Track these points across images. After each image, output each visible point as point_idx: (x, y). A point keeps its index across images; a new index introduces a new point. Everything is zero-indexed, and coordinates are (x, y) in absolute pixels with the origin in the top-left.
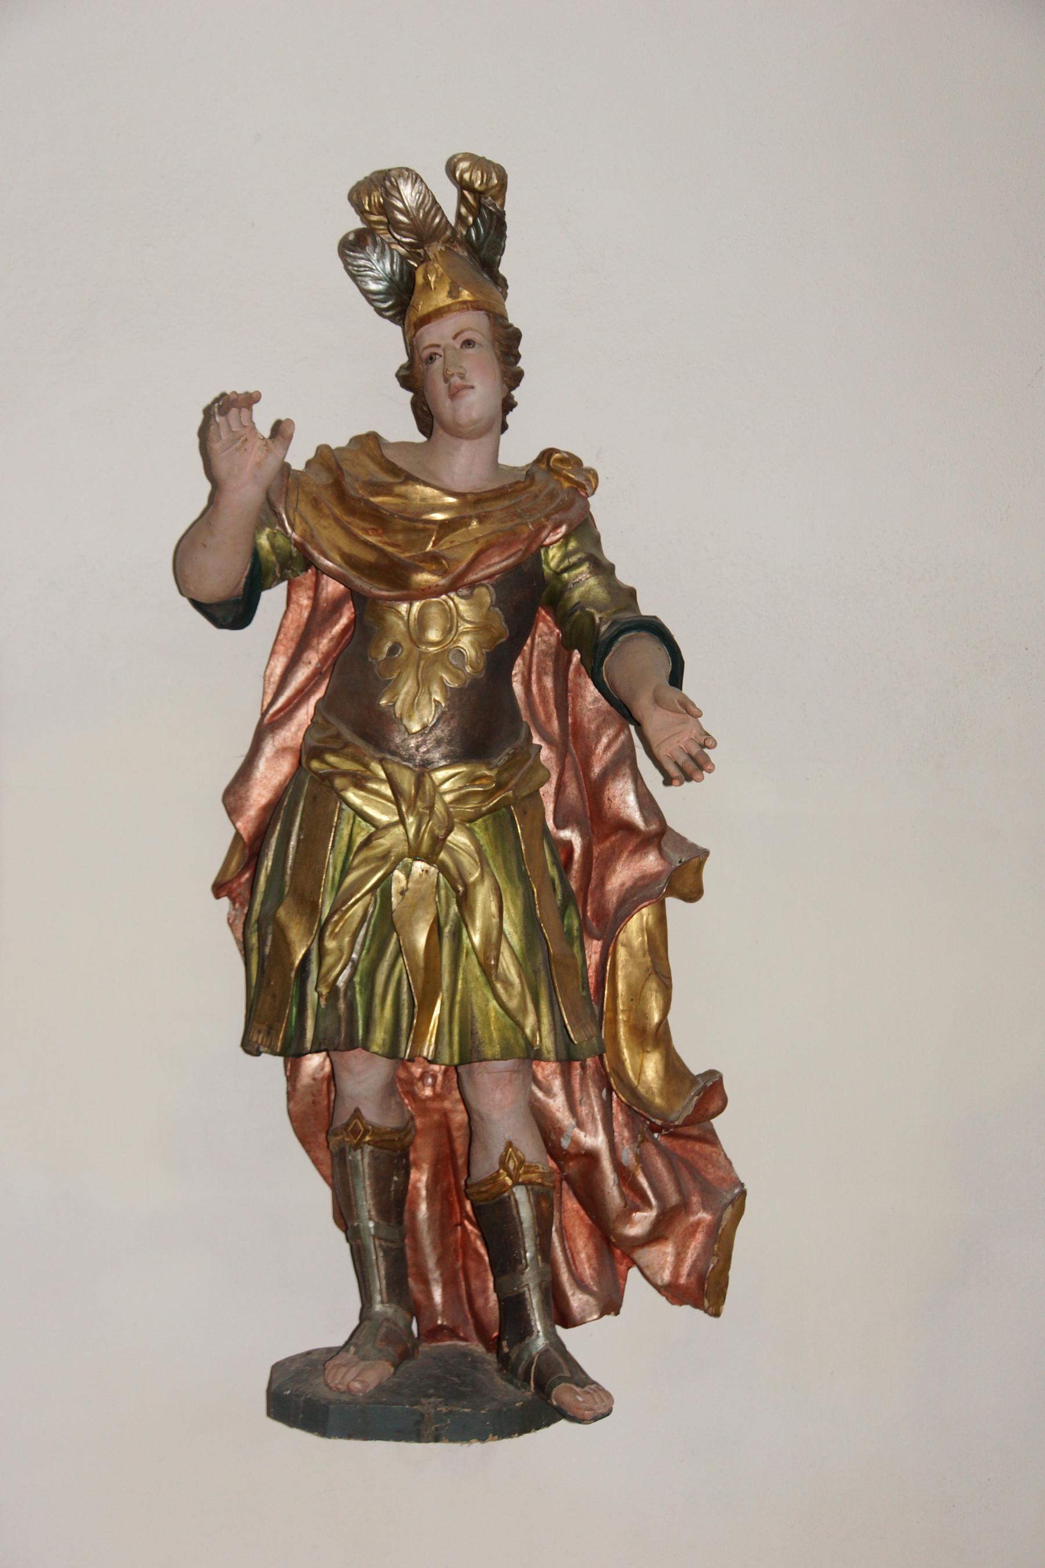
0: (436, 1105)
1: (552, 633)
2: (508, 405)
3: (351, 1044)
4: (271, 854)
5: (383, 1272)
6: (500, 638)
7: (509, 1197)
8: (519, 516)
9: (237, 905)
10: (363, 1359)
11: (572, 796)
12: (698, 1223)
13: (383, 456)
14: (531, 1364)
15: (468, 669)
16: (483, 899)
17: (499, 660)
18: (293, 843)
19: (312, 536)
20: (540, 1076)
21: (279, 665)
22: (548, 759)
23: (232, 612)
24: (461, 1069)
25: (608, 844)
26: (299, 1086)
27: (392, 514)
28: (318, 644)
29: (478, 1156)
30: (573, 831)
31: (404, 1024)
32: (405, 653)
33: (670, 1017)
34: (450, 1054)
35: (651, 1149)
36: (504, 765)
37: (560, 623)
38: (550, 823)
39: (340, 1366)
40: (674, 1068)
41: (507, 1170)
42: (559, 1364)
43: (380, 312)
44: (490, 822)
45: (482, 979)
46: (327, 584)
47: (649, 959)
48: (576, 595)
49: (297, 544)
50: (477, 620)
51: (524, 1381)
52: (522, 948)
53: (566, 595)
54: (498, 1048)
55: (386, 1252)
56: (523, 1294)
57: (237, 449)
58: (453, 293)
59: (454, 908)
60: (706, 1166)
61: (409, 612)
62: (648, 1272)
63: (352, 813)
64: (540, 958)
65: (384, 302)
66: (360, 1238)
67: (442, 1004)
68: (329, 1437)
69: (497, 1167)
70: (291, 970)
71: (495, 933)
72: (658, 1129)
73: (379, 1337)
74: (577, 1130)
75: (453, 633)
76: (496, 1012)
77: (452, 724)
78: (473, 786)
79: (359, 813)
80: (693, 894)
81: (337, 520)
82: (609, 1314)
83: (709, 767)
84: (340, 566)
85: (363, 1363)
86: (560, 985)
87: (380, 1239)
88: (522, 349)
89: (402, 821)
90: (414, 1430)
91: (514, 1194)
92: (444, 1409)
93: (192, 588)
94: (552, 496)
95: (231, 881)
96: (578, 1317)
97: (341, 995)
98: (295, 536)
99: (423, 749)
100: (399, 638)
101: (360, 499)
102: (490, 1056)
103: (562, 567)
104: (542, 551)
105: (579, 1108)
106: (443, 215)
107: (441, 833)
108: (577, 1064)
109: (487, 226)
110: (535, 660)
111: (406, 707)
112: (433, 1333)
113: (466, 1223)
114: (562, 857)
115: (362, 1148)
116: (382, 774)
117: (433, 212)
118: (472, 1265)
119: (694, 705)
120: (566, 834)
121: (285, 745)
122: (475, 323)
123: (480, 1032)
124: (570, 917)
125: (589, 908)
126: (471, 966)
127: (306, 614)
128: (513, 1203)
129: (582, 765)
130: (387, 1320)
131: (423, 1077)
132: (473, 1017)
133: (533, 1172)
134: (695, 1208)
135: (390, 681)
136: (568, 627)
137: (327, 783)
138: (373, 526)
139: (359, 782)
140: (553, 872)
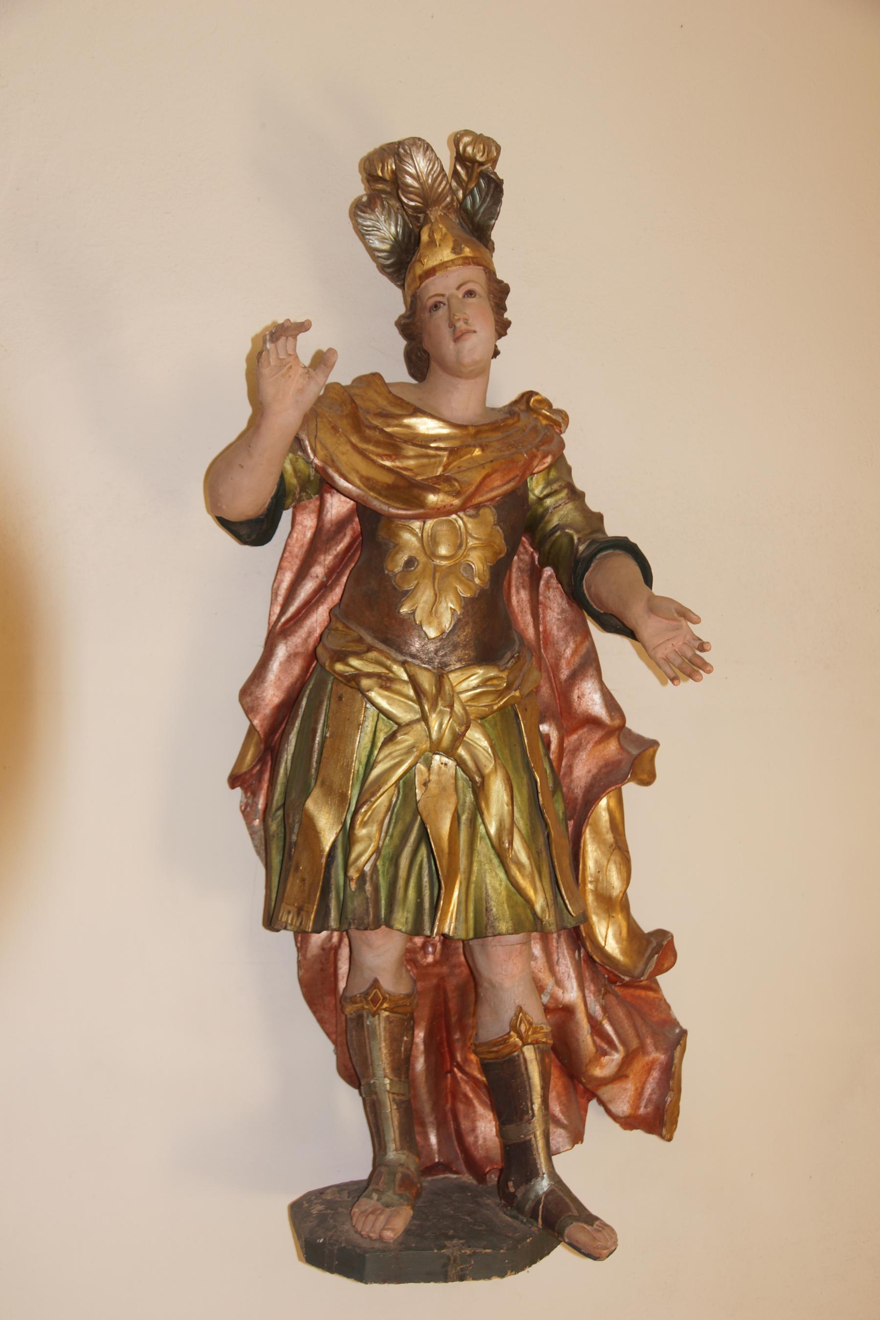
5: (396, 1123)
6: (500, 553)
7: (518, 1056)
9: (249, 794)
10: (387, 1206)
12: (653, 1062)
13: (390, 392)
14: (539, 1202)
15: (477, 581)
16: (497, 790)
19: (333, 461)
21: (288, 578)
30: (550, 726)
32: (420, 567)
42: (566, 1203)
43: (382, 268)
49: (317, 469)
50: (484, 537)
51: (531, 1217)
55: (399, 1104)
57: (283, 376)
58: (456, 250)
61: (422, 529)
64: (541, 840)
66: (376, 1093)
68: (366, 1283)
73: (397, 1183)
74: (556, 988)
75: (463, 548)
80: (647, 778)
83: (708, 669)
84: (358, 487)
85: (388, 1211)
86: (559, 863)
87: (393, 1093)
89: (424, 718)
90: (441, 1274)
91: (523, 1053)
93: (224, 507)
94: (535, 429)
95: (245, 773)
97: (368, 879)
98: (316, 461)
99: (441, 653)
102: (504, 931)
109: (484, 194)
112: (430, 1169)
113: (455, 1069)
116: (405, 677)
117: (440, 178)
118: (461, 1107)
120: (544, 728)
123: (494, 910)
126: (483, 848)
128: (522, 1060)
130: (402, 1165)
131: (424, 946)
133: (539, 1032)
135: (408, 591)
137: (353, 684)
139: (386, 682)
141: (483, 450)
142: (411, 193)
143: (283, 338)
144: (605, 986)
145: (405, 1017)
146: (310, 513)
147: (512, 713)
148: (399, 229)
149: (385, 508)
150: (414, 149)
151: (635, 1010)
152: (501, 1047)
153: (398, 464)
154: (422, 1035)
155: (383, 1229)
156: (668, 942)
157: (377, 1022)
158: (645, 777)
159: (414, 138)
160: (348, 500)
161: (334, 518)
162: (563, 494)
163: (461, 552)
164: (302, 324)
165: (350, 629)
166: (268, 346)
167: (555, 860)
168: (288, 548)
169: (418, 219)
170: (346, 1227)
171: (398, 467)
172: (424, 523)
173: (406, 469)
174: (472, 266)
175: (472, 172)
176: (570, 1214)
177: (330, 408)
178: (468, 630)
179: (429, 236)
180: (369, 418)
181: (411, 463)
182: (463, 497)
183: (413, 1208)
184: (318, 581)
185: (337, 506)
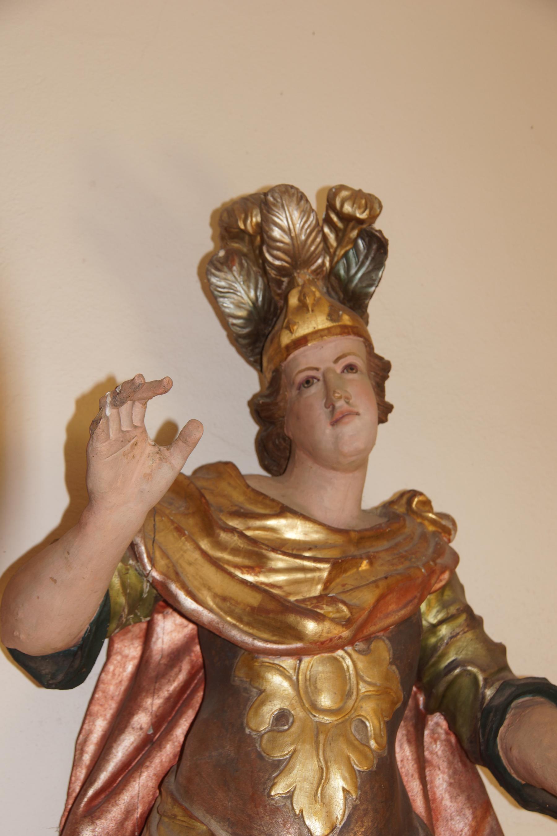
13: (248, 486)
19: (177, 574)
21: (100, 726)
43: (235, 339)
49: (154, 584)
57: (125, 455)
58: (331, 316)
61: (297, 670)
75: (354, 697)
84: (211, 610)
93: (22, 636)
98: (155, 574)
109: (361, 258)
141: (371, 563)
142: (279, 249)
143: (129, 403)
146: (132, 639)
148: (260, 294)
149: (248, 640)
150: (286, 197)
153: (262, 579)
159: (286, 186)
160: (185, 622)
161: (166, 646)
162: (462, 619)
163: (351, 703)
164: (159, 383)
165: (197, 819)
166: (108, 411)
168: (101, 686)
169: (279, 283)
171: (262, 583)
172: (300, 661)
173: (273, 586)
174: (352, 337)
175: (344, 236)
177: (171, 504)
178: (367, 822)
179: (299, 300)
180: (223, 518)
181: (280, 578)
182: (355, 626)
184: (142, 734)
185: (170, 631)
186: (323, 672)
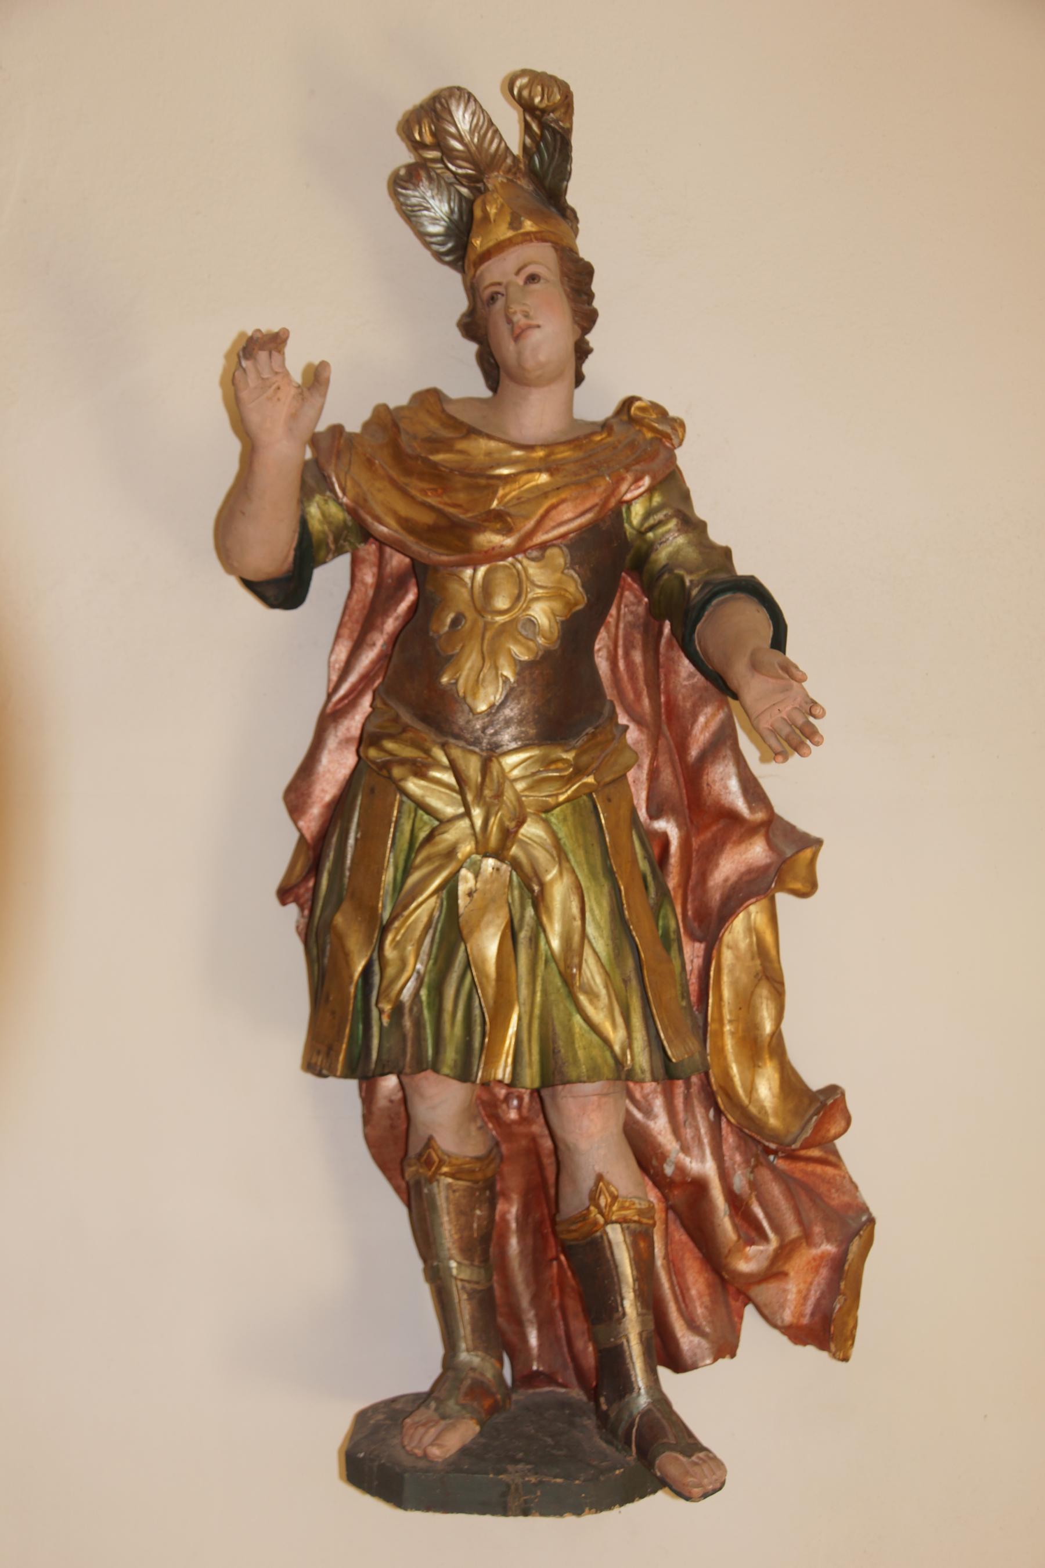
0: (522, 1129)
1: (640, 602)
2: (582, 351)
3: (420, 1065)
4: (332, 855)
6: (576, 604)
8: (592, 467)
10: (443, 1417)
11: (666, 783)
13: (443, 411)
14: (632, 1425)
15: (541, 640)
17: (578, 629)
18: (351, 841)
19: (365, 500)
20: (638, 1095)
21: (342, 653)
22: (637, 742)
23: (284, 590)
24: (546, 1093)
25: (708, 835)
26: (375, 1109)
27: (452, 470)
28: (383, 623)
29: (566, 1190)
30: (668, 821)
31: (477, 1044)
33: (784, 1027)
34: (531, 1077)
35: (765, 1174)
36: (582, 746)
37: (647, 590)
38: (643, 814)
39: (416, 1425)
40: (791, 1083)
41: (598, 1206)
43: (439, 256)
44: (569, 811)
45: (563, 991)
46: (391, 556)
47: (758, 962)
48: (662, 555)
52: (608, 954)
53: (653, 556)
54: (584, 1069)
56: (622, 1344)
57: (269, 399)
58: (515, 223)
59: (530, 911)
60: (829, 1191)
61: (473, 578)
62: (766, 1312)
63: (413, 805)
64: (630, 963)
65: (442, 244)
67: (520, 1019)
68: (405, 1509)
69: (587, 1203)
70: (351, 983)
71: (576, 938)
72: (775, 1152)
74: (682, 1156)
75: (523, 599)
76: (581, 1028)
77: (522, 702)
78: (547, 771)
79: (421, 806)
81: (393, 482)
82: (723, 1357)
83: (816, 739)
84: (396, 531)
85: (443, 1423)
86: (654, 996)
88: (595, 287)
89: (468, 814)
90: (500, 1505)
91: (607, 1234)
92: (533, 1480)
94: (632, 445)
95: (297, 886)
96: (689, 1362)
97: (407, 1010)
98: (345, 500)
99: (490, 731)
100: (462, 607)
101: (417, 457)
103: (646, 525)
104: (624, 510)
105: (682, 1130)
106: (501, 139)
107: (512, 825)
108: (680, 1082)
109: (551, 149)
110: (621, 633)
111: (471, 683)
114: (656, 851)
115: (438, 1181)
116: (445, 760)
117: (489, 135)
119: (797, 667)
120: (661, 825)
121: (348, 735)
122: (541, 257)
123: (563, 1051)
124: (665, 917)
125: (689, 907)
127: (371, 593)
129: (676, 747)
130: (473, 1369)
131: (507, 1099)
132: (555, 1034)
133: (628, 1208)
134: (817, 1239)
135: (452, 656)
136: (656, 593)
137: (384, 772)
138: (431, 486)
139: (420, 771)
140: (644, 865)
141: (552, 474)
144: (756, 1156)
145: (476, 1186)
147: (589, 804)
151: (799, 1190)
152: (579, 1225)
154: (513, 1210)
155: (432, 1444)
156: (835, 1101)
157: (436, 1190)
158: (798, 886)
167: (649, 990)
170: (396, 1441)
176: (665, 1440)
183: (481, 1423)
186: (571, 594)
